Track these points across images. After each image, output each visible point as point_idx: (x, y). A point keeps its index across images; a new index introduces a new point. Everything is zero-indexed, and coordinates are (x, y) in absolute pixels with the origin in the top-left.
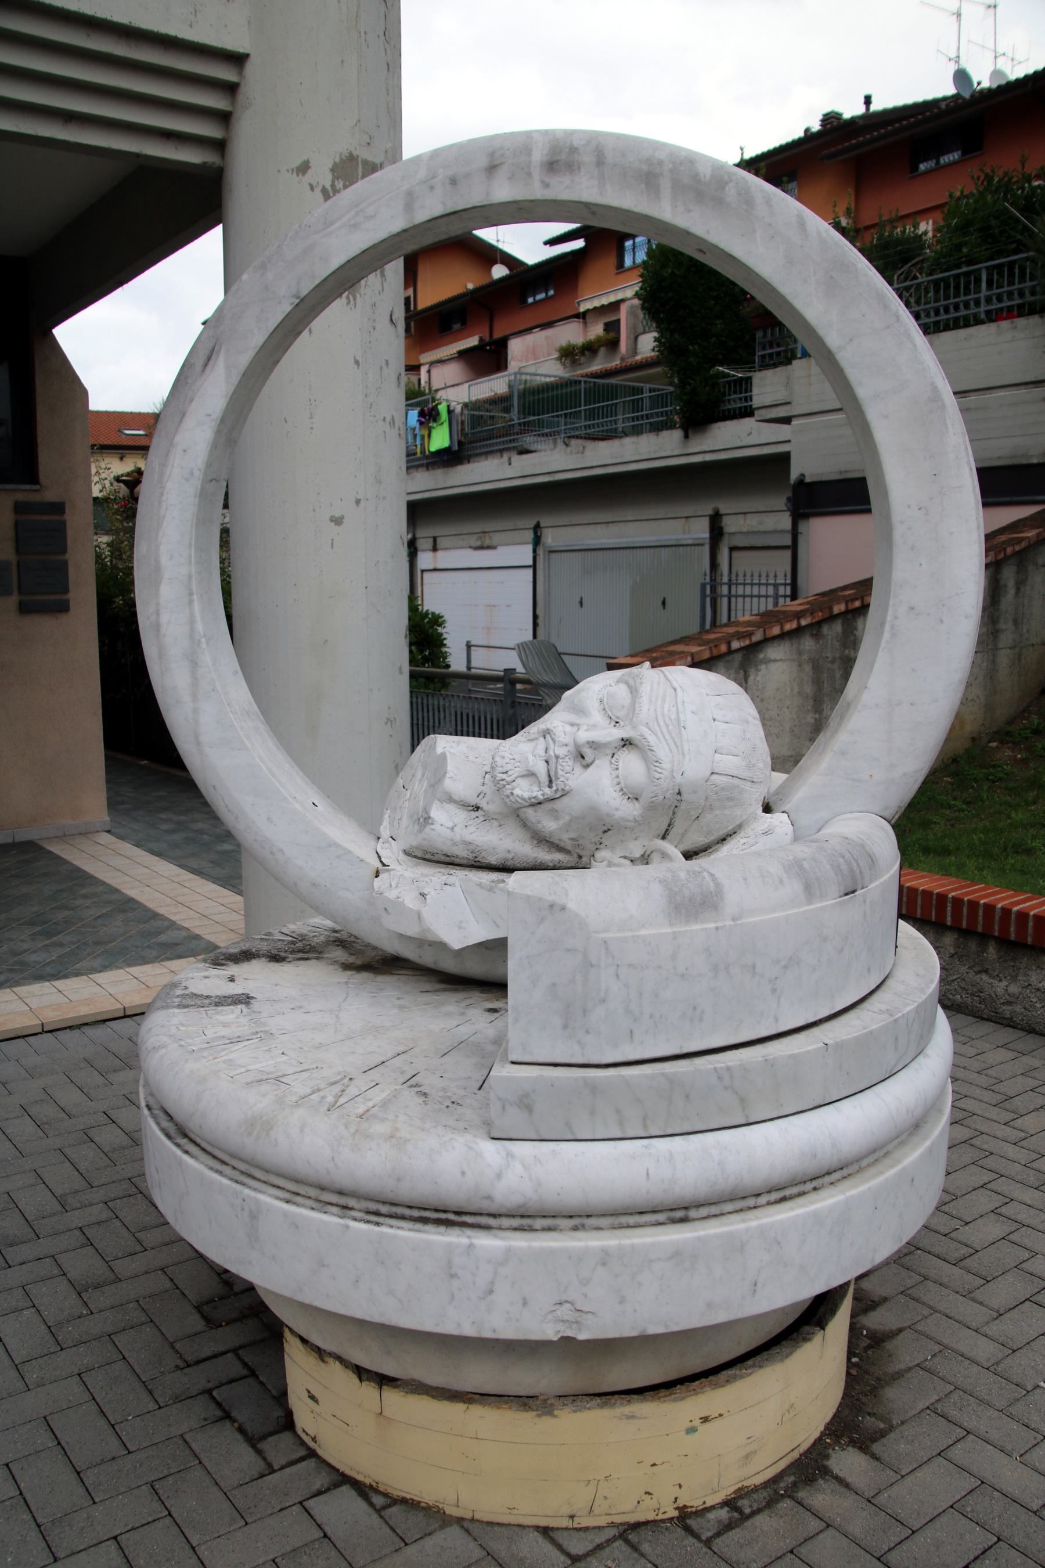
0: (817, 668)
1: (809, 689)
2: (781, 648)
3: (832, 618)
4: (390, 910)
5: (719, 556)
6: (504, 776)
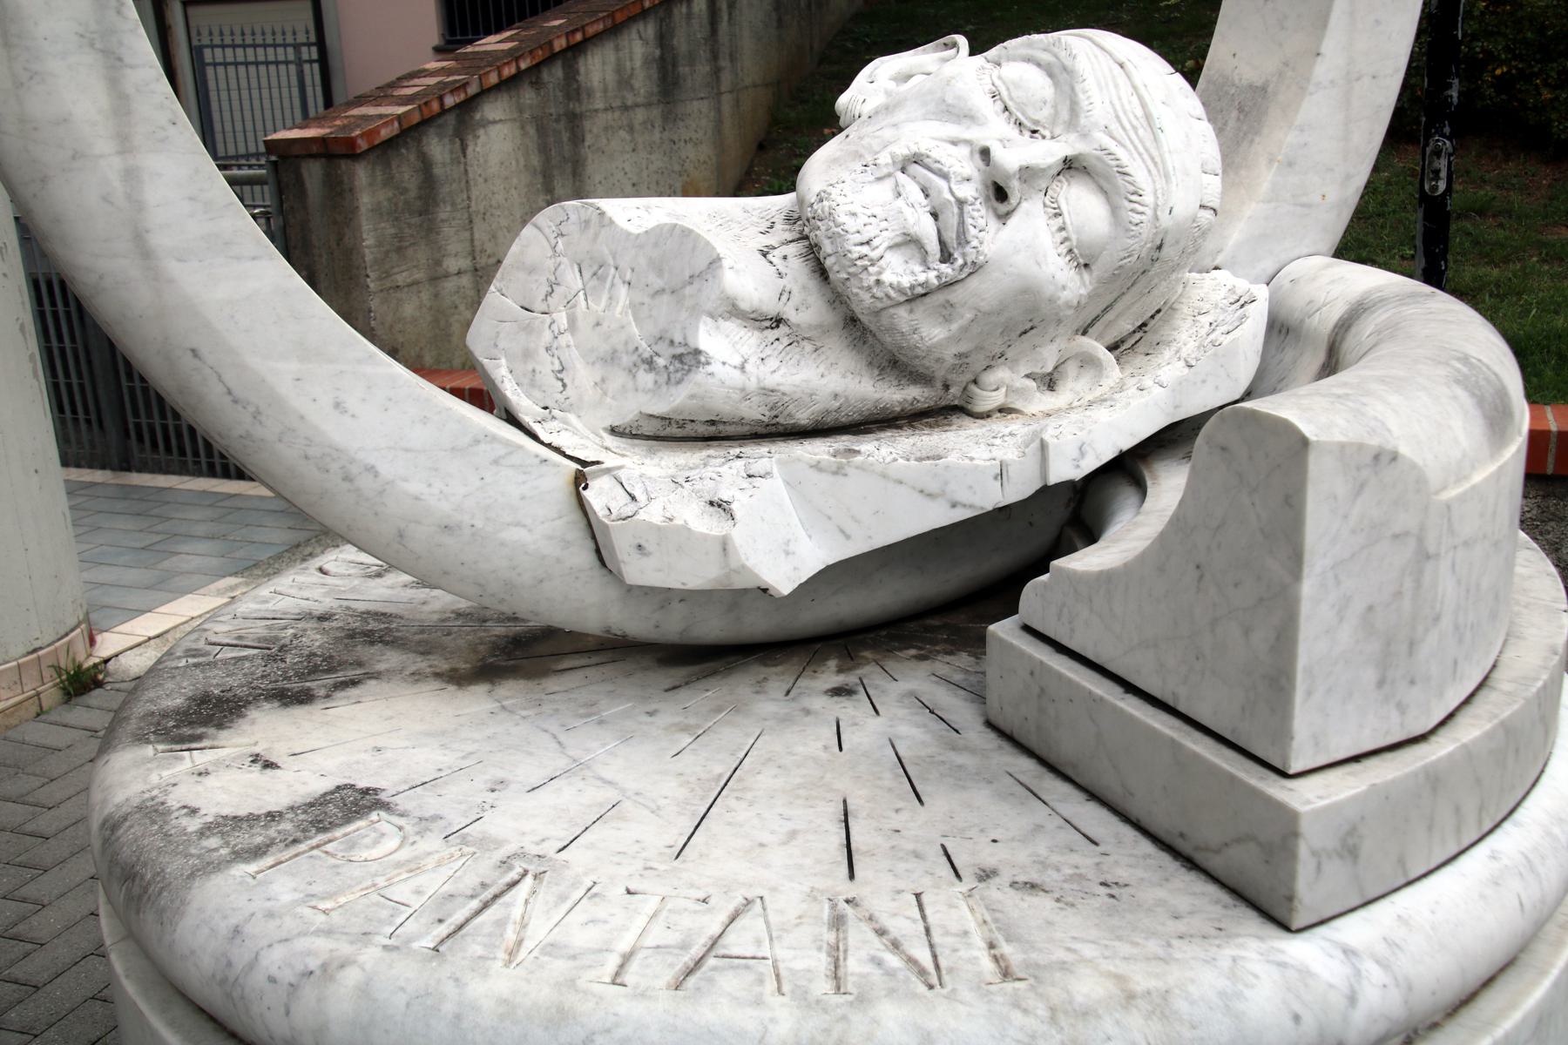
0: (542, 131)
1: (535, 161)
2: (499, 104)
3: (551, 58)
4: (649, 547)
5: (168, 14)
6: (865, 250)
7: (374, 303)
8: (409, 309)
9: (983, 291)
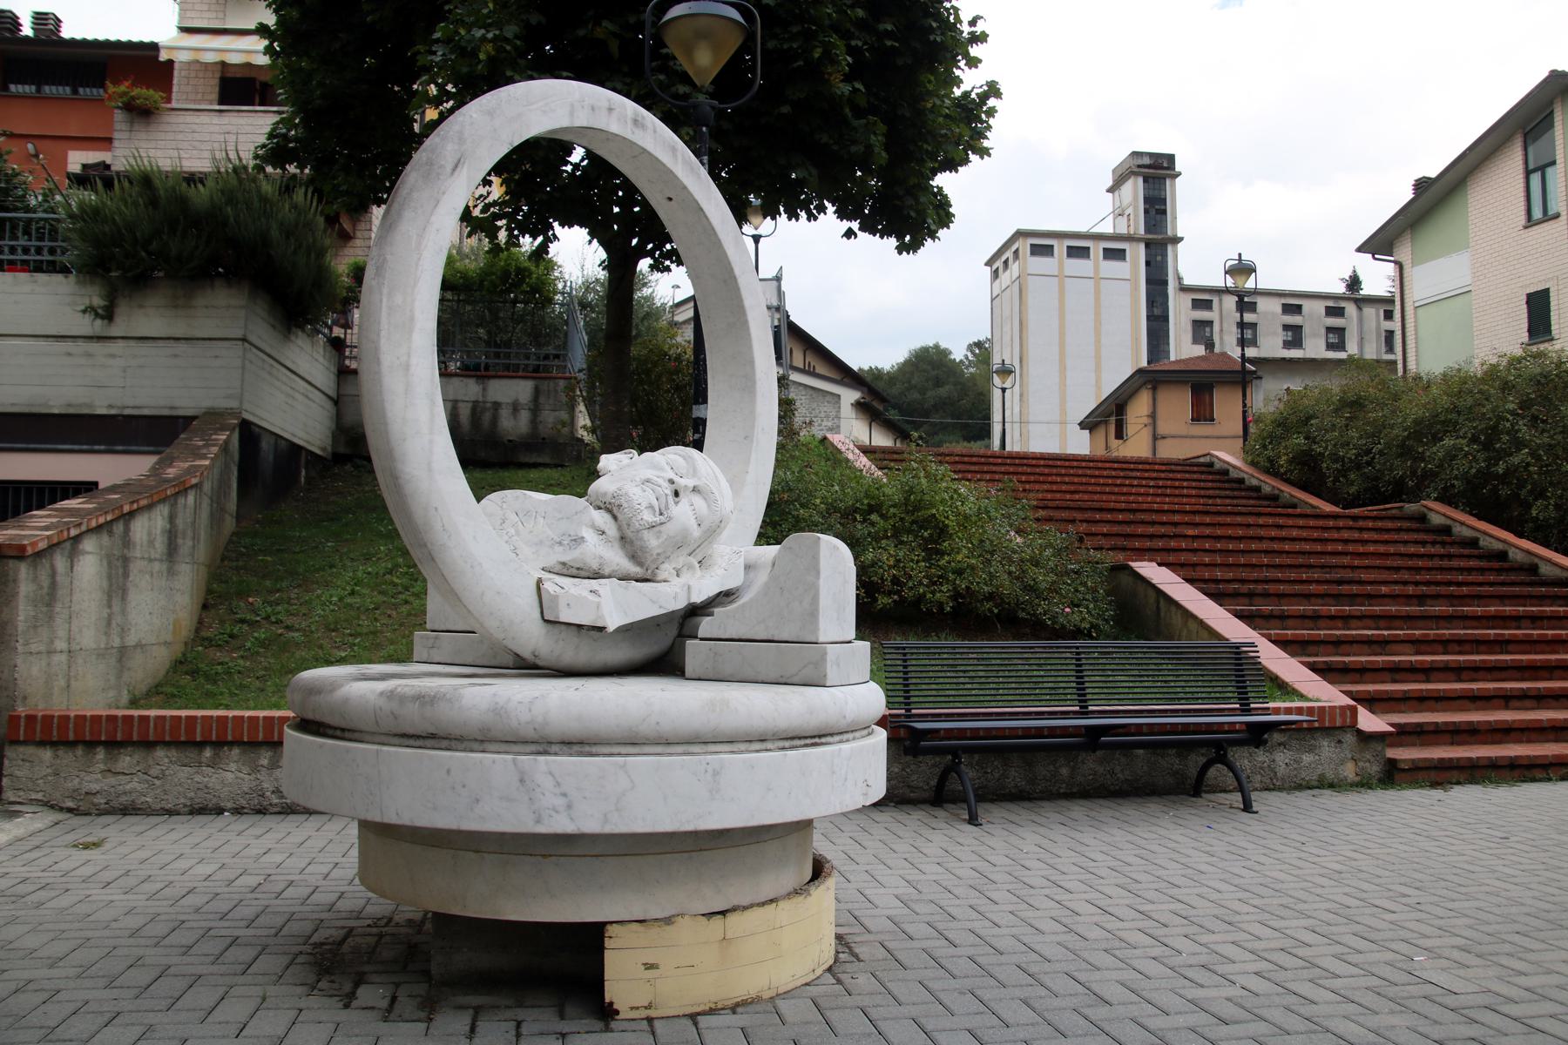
0: (109, 563)
1: (105, 584)
7: (19, 661)
8: (35, 671)
9: (670, 529)
